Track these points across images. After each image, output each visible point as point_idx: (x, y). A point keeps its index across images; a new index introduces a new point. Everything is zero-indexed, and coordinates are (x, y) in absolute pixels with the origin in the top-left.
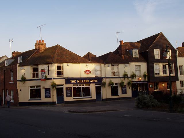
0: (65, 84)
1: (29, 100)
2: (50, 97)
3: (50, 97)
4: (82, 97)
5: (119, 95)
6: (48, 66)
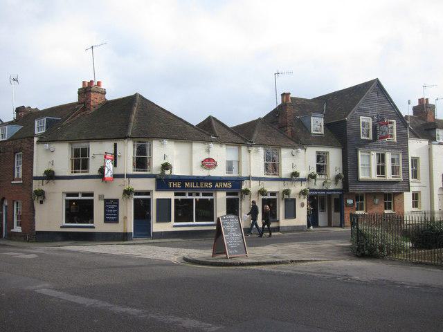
2: (116, 221)
3: (116, 221)
4: (195, 223)
6: (115, 145)
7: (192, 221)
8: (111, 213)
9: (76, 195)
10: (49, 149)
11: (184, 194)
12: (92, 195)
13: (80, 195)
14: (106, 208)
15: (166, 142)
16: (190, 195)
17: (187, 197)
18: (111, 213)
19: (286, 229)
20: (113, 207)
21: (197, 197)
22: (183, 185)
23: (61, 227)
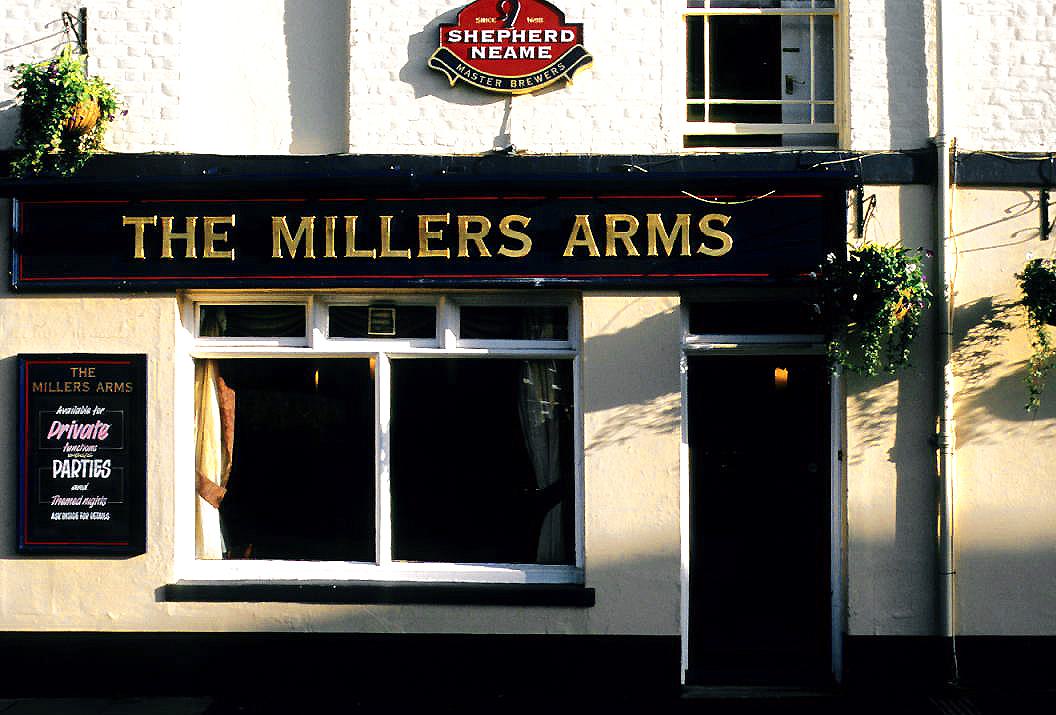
4: (387, 569)
6: (785, 50)
7: (365, 552)
11: (292, 323)
16: (345, 324)
17: (322, 343)
19: (198, 395)
21: (406, 348)
22: (252, 240)
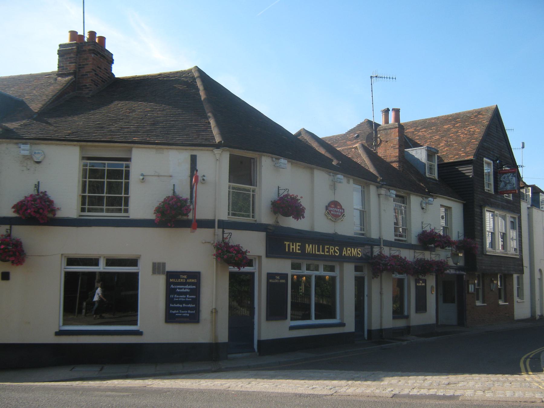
0: (264, 260)
1: (60, 333)
2: (194, 318)
3: (194, 318)
4: (313, 321)
5: (407, 317)
6: (194, 159)
7: (308, 317)
8: (181, 302)
9: (94, 262)
10: (28, 158)
12: (133, 262)
13: (102, 262)
14: (170, 291)
15: (283, 161)
18: (181, 302)
20: (186, 289)
23: (540, 270)
